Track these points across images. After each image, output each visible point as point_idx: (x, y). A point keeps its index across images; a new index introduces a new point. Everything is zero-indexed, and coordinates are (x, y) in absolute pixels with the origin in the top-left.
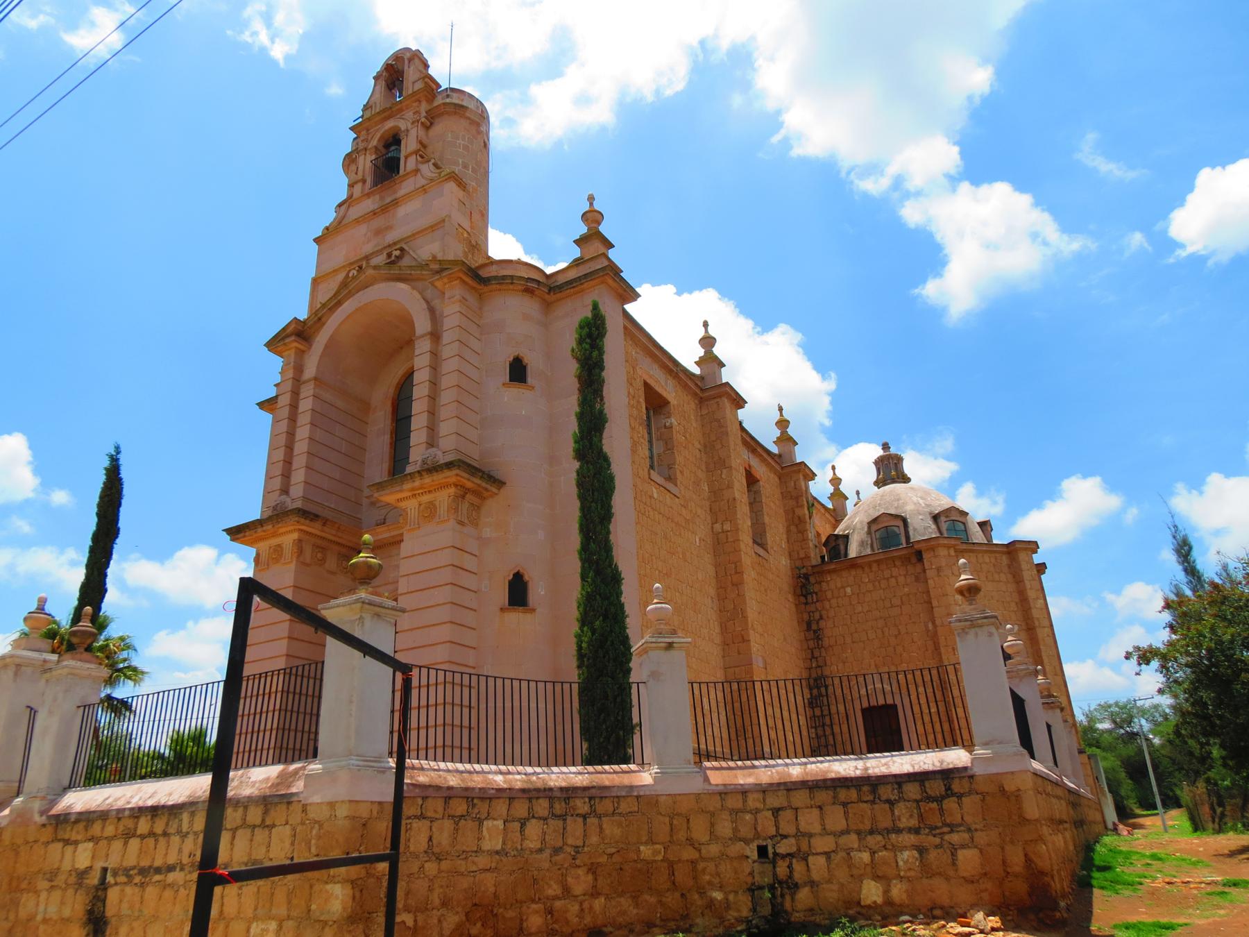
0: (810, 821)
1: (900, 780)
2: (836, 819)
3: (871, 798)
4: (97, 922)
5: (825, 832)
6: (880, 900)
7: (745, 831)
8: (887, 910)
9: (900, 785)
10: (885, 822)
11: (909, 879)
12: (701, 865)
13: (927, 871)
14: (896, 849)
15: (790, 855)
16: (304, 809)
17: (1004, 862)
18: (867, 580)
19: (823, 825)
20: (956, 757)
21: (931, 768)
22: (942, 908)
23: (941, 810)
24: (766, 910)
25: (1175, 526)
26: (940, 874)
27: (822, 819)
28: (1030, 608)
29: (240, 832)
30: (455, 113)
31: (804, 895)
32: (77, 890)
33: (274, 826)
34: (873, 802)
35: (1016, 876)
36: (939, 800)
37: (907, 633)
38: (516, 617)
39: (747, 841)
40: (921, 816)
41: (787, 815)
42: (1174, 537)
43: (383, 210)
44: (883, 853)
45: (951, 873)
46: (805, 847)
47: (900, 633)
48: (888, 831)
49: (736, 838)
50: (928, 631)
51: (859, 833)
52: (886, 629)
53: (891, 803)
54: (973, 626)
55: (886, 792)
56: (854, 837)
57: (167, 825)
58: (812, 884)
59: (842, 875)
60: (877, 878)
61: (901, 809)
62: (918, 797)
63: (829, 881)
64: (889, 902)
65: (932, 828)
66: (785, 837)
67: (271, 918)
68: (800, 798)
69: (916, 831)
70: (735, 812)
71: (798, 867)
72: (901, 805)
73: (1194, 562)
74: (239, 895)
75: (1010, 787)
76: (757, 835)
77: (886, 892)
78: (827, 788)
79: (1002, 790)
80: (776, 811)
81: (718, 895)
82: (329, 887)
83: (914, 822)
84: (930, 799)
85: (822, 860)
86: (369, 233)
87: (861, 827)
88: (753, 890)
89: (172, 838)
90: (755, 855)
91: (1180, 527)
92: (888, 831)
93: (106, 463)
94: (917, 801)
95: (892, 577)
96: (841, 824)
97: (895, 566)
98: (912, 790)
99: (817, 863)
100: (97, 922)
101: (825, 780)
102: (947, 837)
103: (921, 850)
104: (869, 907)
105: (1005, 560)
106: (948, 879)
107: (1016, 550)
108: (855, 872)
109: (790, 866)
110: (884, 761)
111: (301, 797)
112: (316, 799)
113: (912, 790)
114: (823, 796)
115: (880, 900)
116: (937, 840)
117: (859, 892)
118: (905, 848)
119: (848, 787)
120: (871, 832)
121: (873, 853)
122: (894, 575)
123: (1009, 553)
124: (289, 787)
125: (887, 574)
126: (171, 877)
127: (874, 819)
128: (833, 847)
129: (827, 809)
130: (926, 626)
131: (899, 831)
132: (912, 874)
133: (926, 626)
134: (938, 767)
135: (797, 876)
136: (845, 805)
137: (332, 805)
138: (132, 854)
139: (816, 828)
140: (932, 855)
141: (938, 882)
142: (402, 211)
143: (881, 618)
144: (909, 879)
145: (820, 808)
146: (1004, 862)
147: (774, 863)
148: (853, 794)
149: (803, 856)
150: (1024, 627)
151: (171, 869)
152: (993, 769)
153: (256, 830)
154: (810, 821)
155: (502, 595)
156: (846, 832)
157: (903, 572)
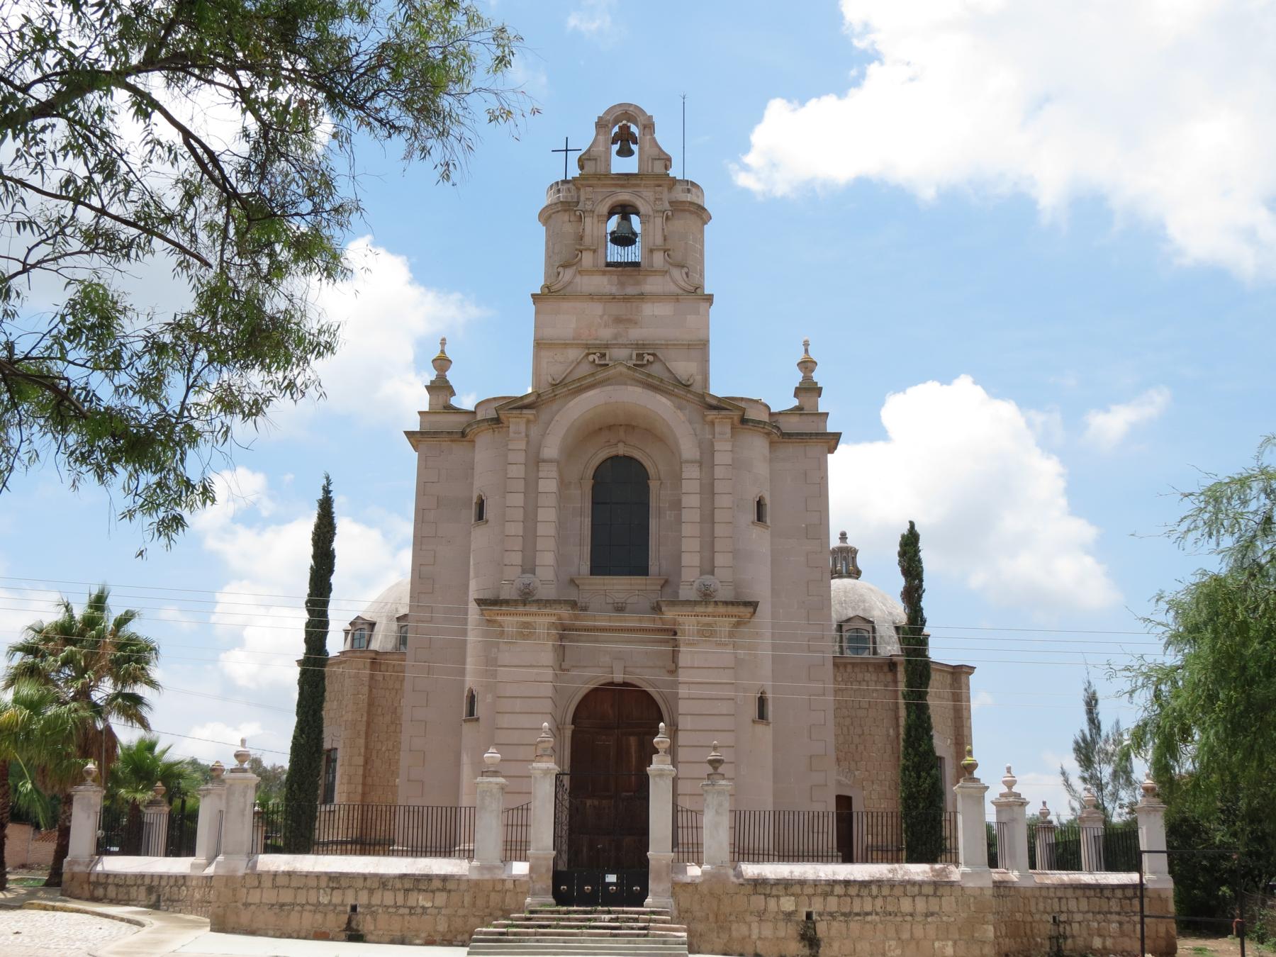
0: (1073, 905)
1: (1114, 888)
2: (1084, 905)
3: (1099, 895)
4: (810, 939)
5: (1079, 911)
6: (1100, 947)
7: (1049, 909)
8: (1103, 952)
9: (1113, 889)
10: (1106, 909)
11: (1114, 937)
12: (1034, 924)
13: (1123, 934)
14: (1109, 922)
15: (1065, 922)
16: (963, 888)
17: (1157, 931)
18: (840, 679)
19: (1078, 907)
20: (1133, 878)
21: (1127, 883)
22: (1127, 952)
23: (1131, 904)
24: (1055, 949)
25: (1089, 682)
26: (1127, 936)
27: (1078, 904)
28: (963, 726)
29: (917, 899)
30: (695, 213)
31: (1070, 941)
32: (787, 923)
33: (943, 896)
34: (1100, 898)
35: (1161, 938)
36: (1130, 899)
37: (870, 734)
38: (760, 728)
39: (1048, 913)
40: (1121, 906)
41: (1064, 901)
42: (1086, 690)
43: (624, 299)
44: (1103, 924)
45: (1132, 935)
46: (1070, 919)
47: (863, 734)
48: (1107, 913)
49: (1045, 912)
50: (888, 735)
51: (1093, 913)
52: (852, 728)
53: (1108, 898)
54: (1153, 811)
55: (1107, 893)
56: (1091, 914)
57: (859, 890)
58: (1073, 937)
59: (1085, 934)
60: (1100, 936)
61: (1113, 902)
62: (1121, 896)
63: (1080, 936)
64: (1104, 948)
65: (1126, 913)
66: (1062, 912)
67: (949, 939)
68: (1070, 893)
69: (1119, 914)
70: (1045, 898)
71: (1068, 928)
72: (1113, 900)
73: (1097, 714)
74: (252, 921)
75: (1163, 896)
76: (1053, 911)
77: (1104, 943)
78: (1081, 888)
79: (1159, 896)
80: (1060, 899)
81: (1039, 940)
82: (985, 926)
83: (1118, 909)
84: (1126, 898)
85: (1077, 925)
86: (606, 317)
87: (1094, 910)
88: (1050, 938)
89: (865, 899)
90: (1052, 921)
91: (1092, 684)
92: (1107, 913)
93: (320, 495)
94: (1120, 899)
95: (864, 680)
96: (1086, 908)
97: (868, 671)
98: (1119, 893)
99: (1075, 926)
100: (810, 939)
101: (1080, 884)
102: (1132, 918)
103: (1121, 923)
104: (1096, 950)
105: (948, 679)
106: (1131, 938)
107: (960, 673)
108: (1091, 932)
109: (1065, 928)
110: (1103, 876)
111: (961, 883)
112: (971, 885)
113: (1119, 893)
114: (1079, 893)
115: (1100, 947)
116: (1128, 919)
117: (1092, 942)
118: (1113, 922)
119: (1090, 889)
120: (1099, 913)
121: (1099, 923)
122: (866, 679)
123: (952, 673)
124: (1166, 900)
125: (860, 676)
126: (869, 918)
127: (1100, 906)
128: (1082, 919)
129: (1081, 899)
130: (888, 731)
131: (1111, 913)
132: (1115, 935)
133: (888, 731)
134: (1130, 882)
135: (1068, 933)
136: (1088, 898)
137: (981, 889)
138: (832, 904)
139: (1075, 909)
140: (1126, 926)
141: (1127, 940)
142: (649, 309)
143: (849, 716)
144: (1114, 937)
145: (1077, 899)
146: (1157, 931)
147: (1058, 925)
148: (1092, 893)
149: (1069, 922)
150: (954, 741)
151: (867, 914)
152: (1158, 886)
153: (916, 899)
154: (1073, 905)
155: (753, 711)
156: (1088, 912)
157: (874, 678)
